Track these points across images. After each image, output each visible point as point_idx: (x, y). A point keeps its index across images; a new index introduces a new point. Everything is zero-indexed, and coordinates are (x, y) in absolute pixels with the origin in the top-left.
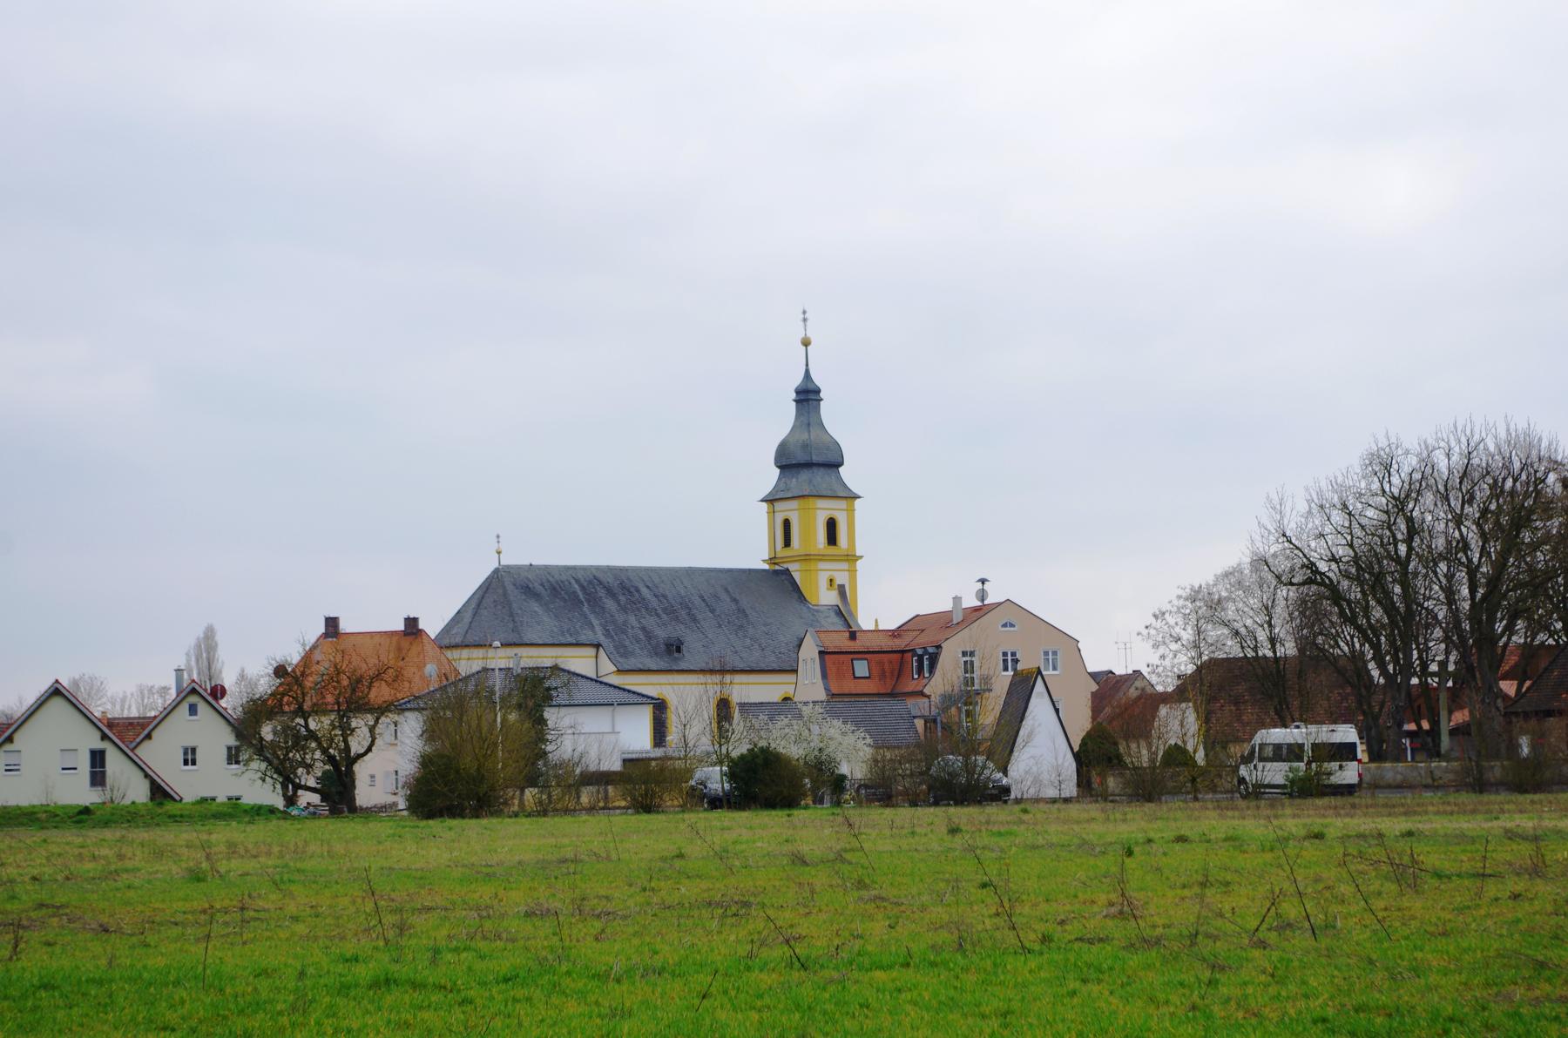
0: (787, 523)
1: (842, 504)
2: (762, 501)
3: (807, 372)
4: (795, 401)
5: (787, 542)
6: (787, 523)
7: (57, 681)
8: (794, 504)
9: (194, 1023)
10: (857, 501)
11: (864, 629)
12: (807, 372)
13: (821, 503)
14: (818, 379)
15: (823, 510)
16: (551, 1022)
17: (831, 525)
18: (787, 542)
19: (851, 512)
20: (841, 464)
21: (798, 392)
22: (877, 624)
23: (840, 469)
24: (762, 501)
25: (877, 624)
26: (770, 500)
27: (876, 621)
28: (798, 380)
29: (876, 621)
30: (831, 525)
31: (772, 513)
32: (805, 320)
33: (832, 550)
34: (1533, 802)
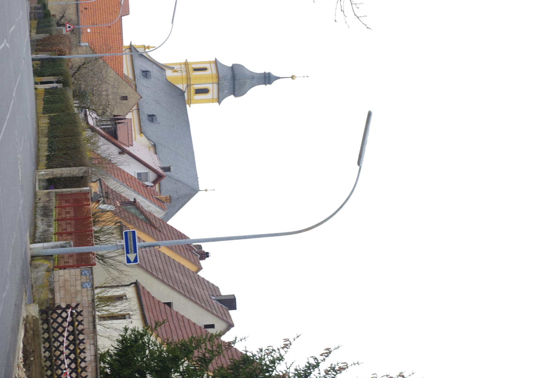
0: (204, 69)
1: (215, 96)
2: (216, 59)
3: (279, 78)
4: (265, 72)
5: (196, 70)
6: (204, 69)
7: (172, 302)
8: (214, 72)
9: (83, 29)
10: (217, 104)
11: (222, 295)
12: (279, 78)
13: (215, 86)
14: (275, 83)
15: (213, 88)
16: (99, 94)
17: (205, 91)
18: (196, 70)
19: (212, 101)
20: (236, 95)
21: (269, 74)
22: (283, 356)
23: (232, 96)
24: (216, 59)
25: (283, 356)
26: (216, 62)
27: (246, 341)
28: (275, 73)
29: (246, 341)
30: (205, 91)
31: (210, 62)
32: (304, 77)
33: (193, 92)
34: (109, 283)
